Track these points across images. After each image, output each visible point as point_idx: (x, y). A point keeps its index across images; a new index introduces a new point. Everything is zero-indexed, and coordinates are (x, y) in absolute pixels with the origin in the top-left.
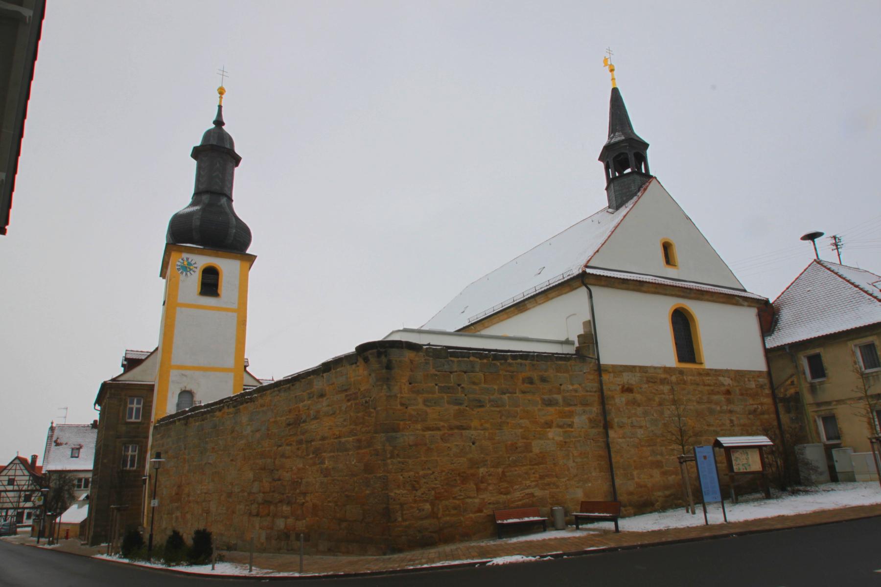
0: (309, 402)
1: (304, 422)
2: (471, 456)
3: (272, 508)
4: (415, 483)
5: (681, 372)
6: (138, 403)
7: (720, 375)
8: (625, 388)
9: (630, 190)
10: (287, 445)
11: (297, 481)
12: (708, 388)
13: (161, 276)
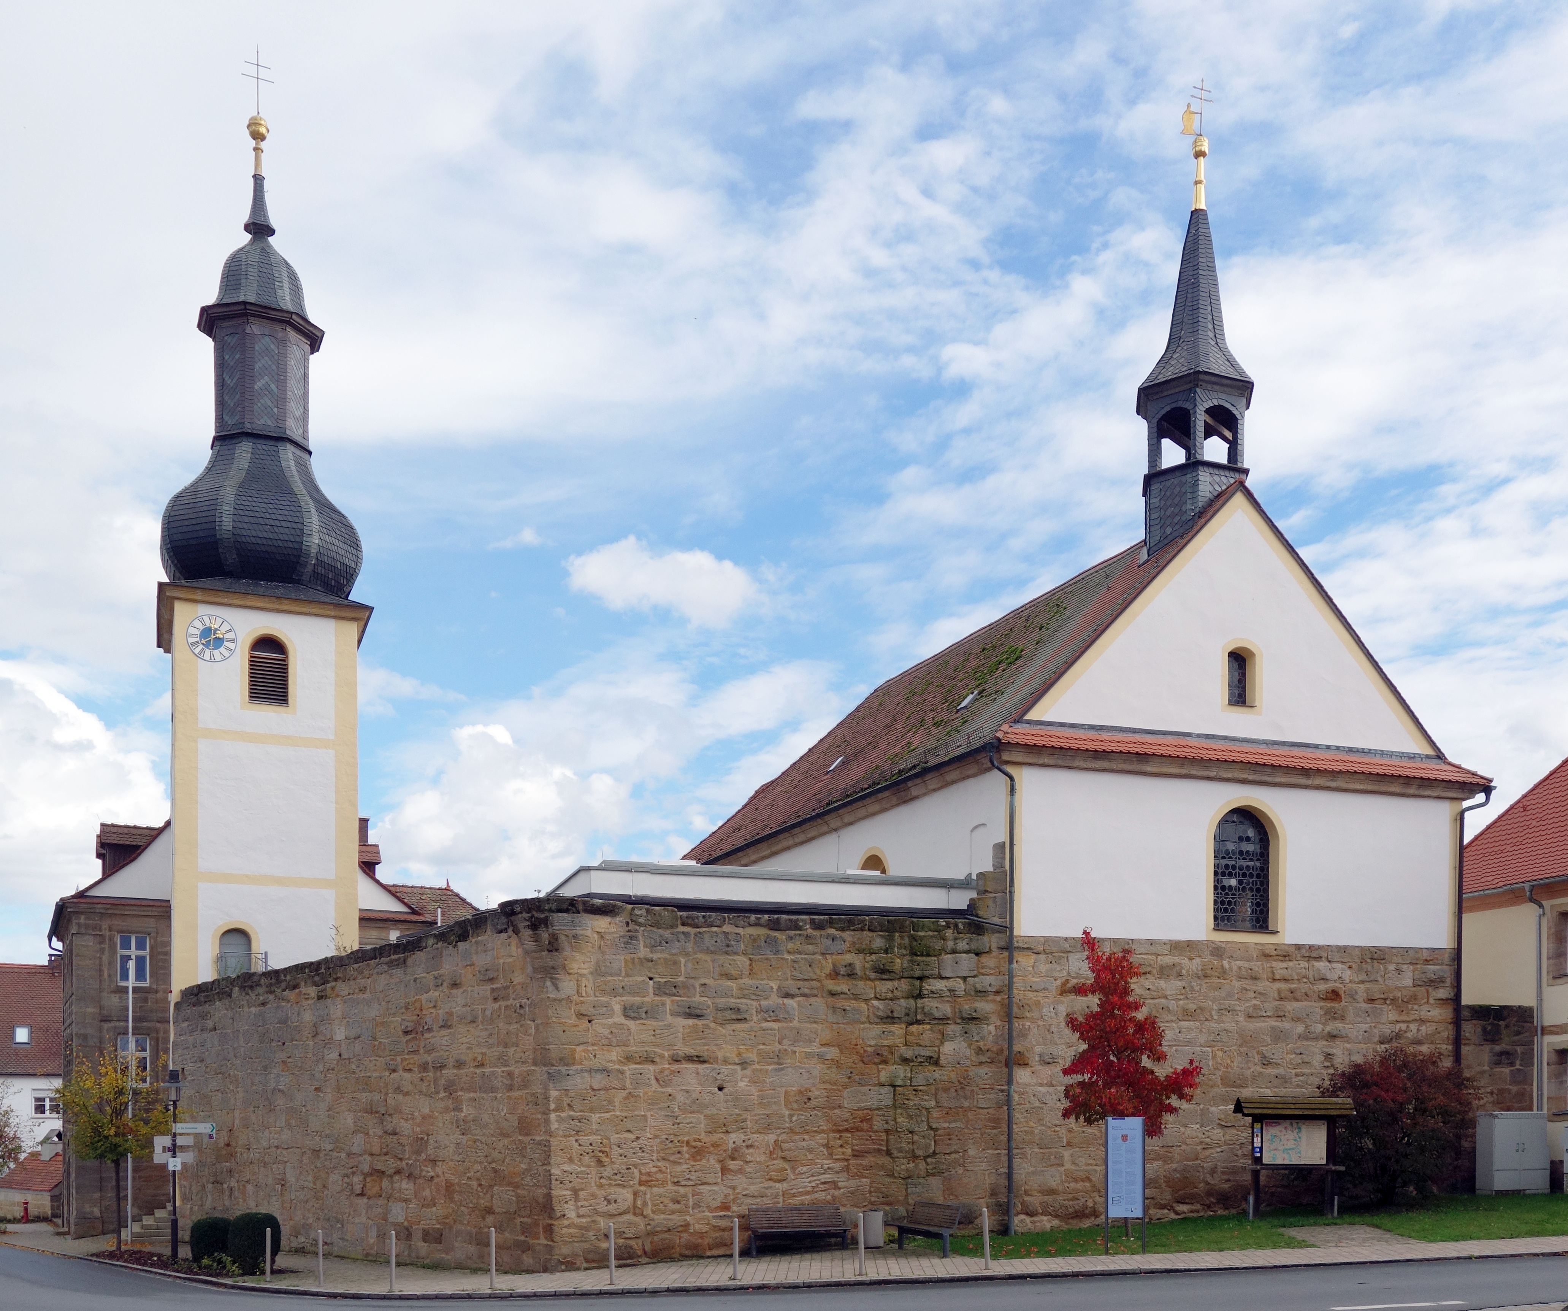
0: (437, 994)
1: (430, 1030)
2: (713, 1111)
3: (385, 1183)
4: (601, 1154)
5: (1217, 951)
6: (140, 946)
7: (1321, 957)
8: (1069, 985)
9: (1183, 509)
10: (405, 1070)
11: (422, 1139)
12: (1283, 986)
13: (159, 646)
